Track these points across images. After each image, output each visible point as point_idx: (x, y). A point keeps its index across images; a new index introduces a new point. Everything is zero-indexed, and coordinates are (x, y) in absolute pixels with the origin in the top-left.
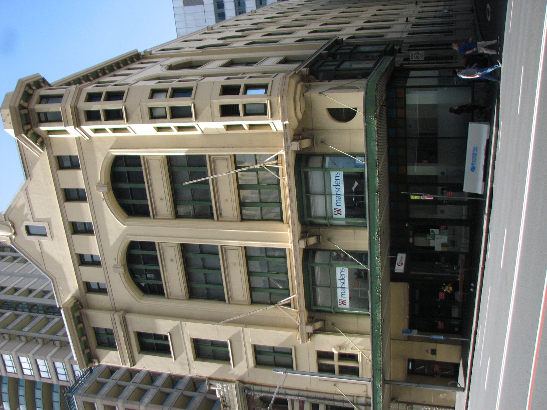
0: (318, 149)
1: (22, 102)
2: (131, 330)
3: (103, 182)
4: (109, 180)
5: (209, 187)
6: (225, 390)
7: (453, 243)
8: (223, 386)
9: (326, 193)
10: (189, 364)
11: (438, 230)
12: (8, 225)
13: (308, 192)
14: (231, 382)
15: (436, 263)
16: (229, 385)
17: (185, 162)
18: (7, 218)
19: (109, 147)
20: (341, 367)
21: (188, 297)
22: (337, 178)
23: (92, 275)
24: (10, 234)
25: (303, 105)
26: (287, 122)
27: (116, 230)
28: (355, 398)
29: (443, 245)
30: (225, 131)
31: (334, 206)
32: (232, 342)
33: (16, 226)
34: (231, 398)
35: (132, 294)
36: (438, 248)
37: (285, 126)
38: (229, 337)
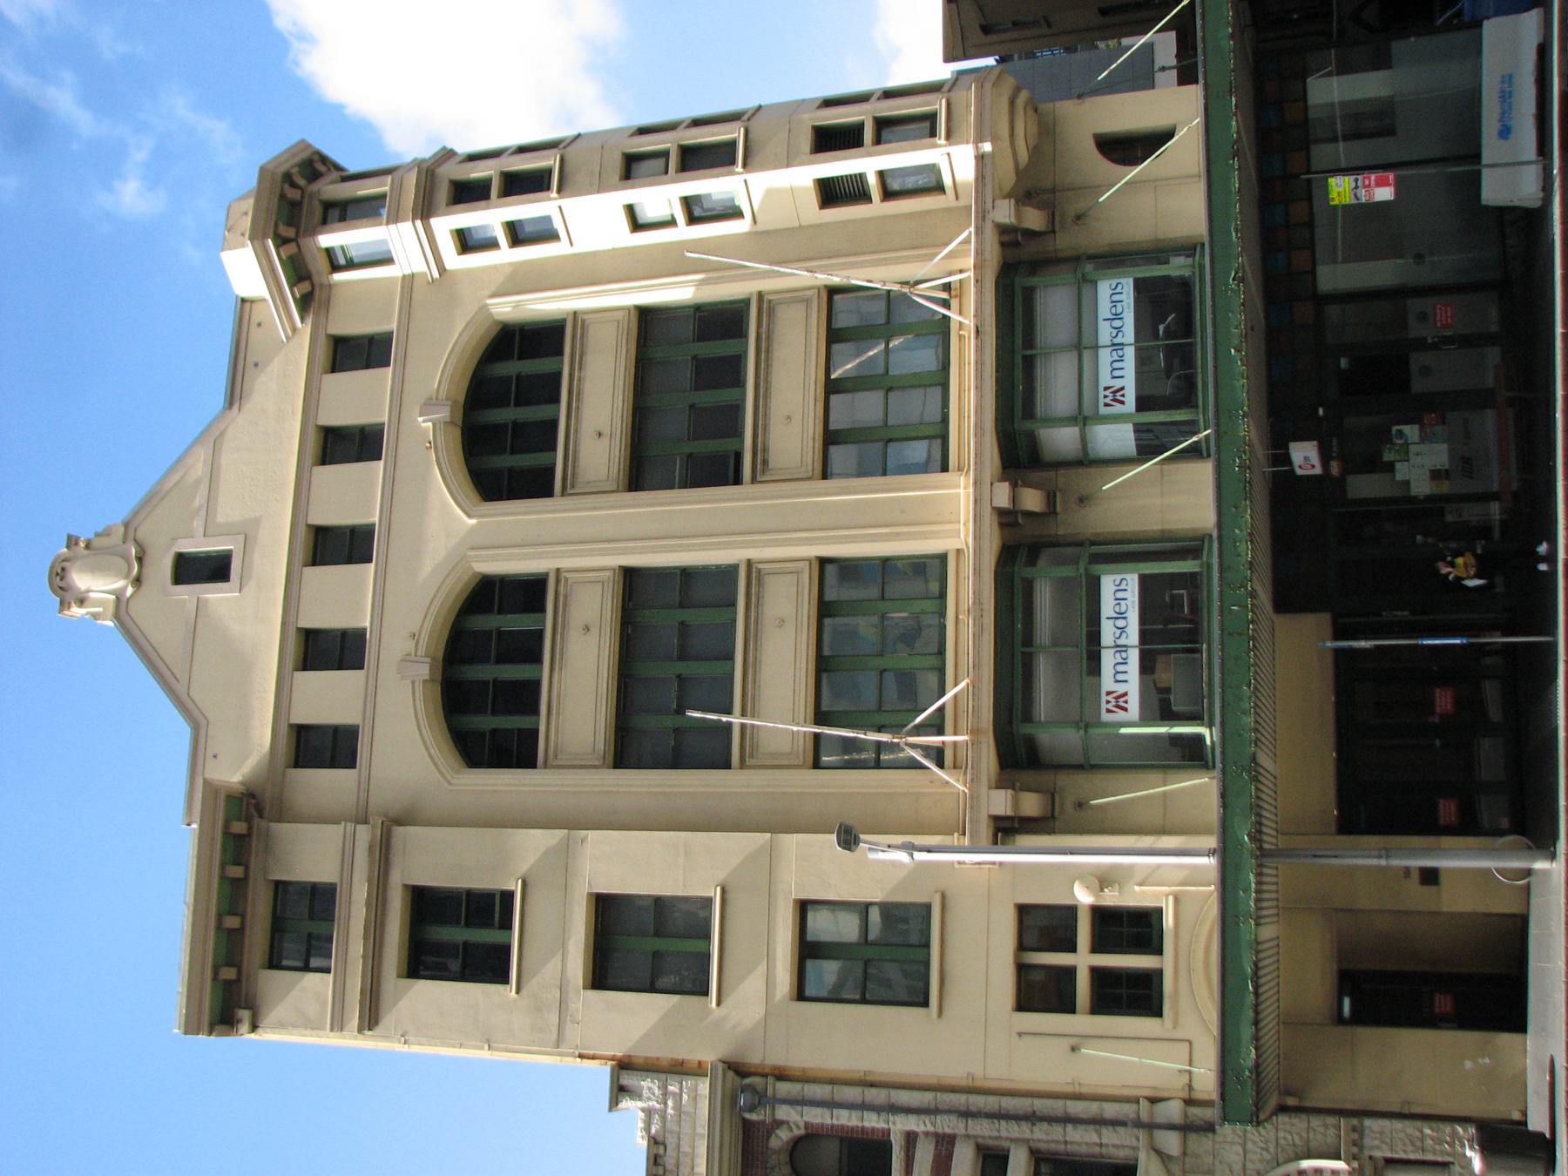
0: (1065, 241)
1: (295, 171)
2: (399, 879)
3: (443, 394)
4: (461, 398)
5: (744, 394)
6: (670, 1111)
7: (1466, 464)
8: (665, 1094)
9: (1083, 345)
10: (562, 1004)
11: (1416, 428)
12: (127, 559)
13: (1029, 341)
14: (698, 1071)
15: (1419, 538)
16: (688, 1083)
17: (689, 329)
18: (131, 535)
19: (488, 293)
20: (1098, 974)
21: (610, 759)
22: (1120, 595)
23: (328, 697)
24: (120, 584)
25: (1033, 129)
26: (987, 147)
27: (445, 532)
28: (1144, 1104)
29: (1436, 475)
30: (811, 211)
31: (1105, 379)
32: (730, 896)
33: (147, 560)
34: (685, 1148)
35: (435, 752)
36: (1422, 487)
37: (980, 158)
38: (721, 876)
